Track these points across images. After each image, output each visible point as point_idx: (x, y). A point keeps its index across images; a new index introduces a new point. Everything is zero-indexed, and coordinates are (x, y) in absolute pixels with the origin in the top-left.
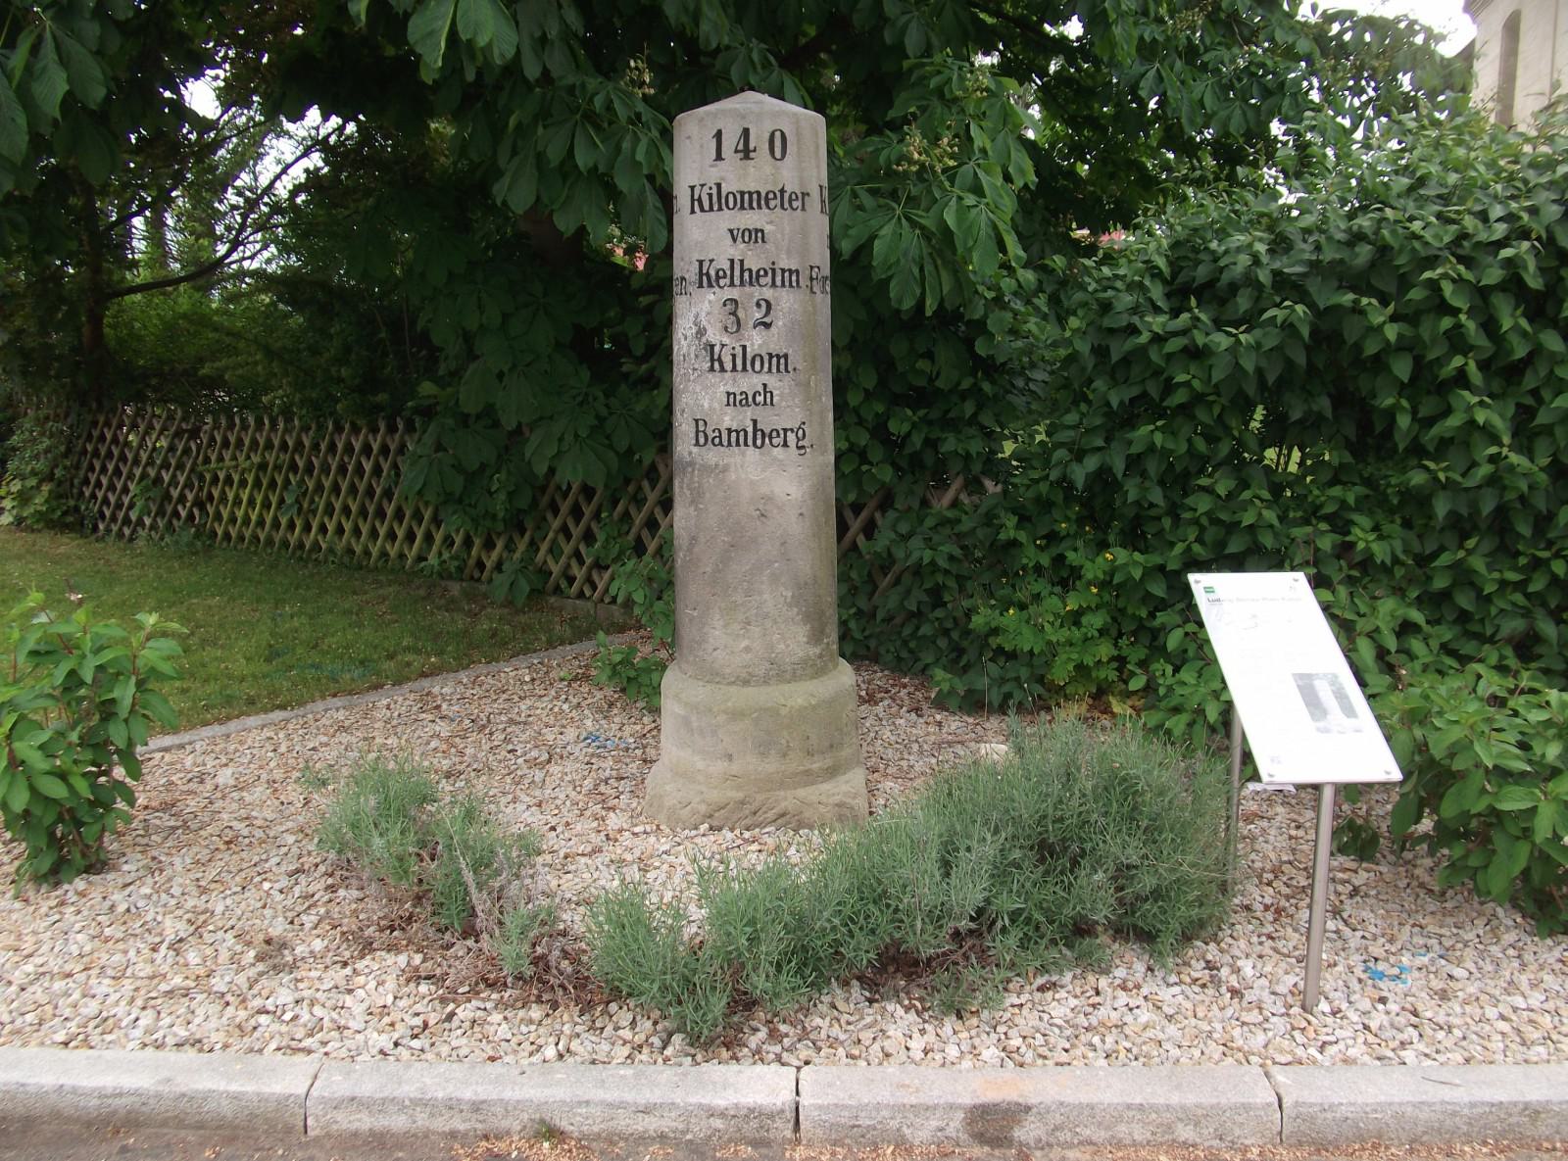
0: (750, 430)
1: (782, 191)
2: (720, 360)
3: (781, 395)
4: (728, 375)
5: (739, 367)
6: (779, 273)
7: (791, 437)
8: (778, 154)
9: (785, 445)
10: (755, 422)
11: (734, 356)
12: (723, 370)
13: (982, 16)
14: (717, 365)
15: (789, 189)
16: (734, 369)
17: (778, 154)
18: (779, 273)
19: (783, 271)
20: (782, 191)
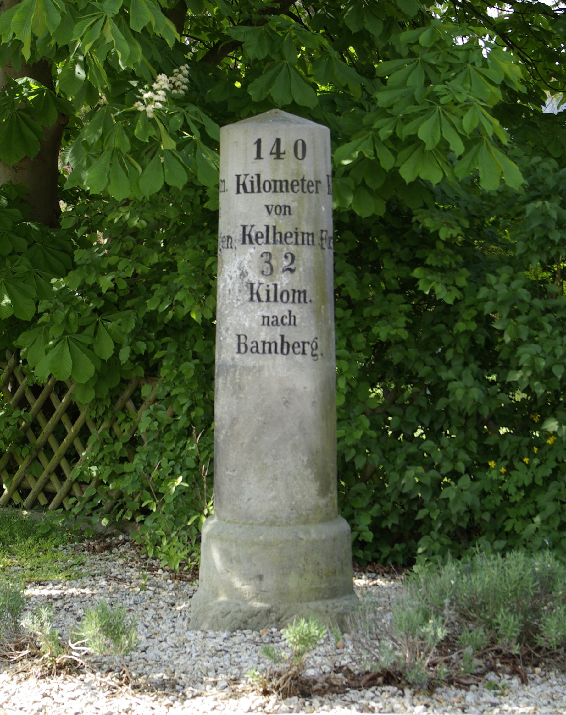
1: (303, 180)
3: (302, 318)
7: (308, 348)
9: (304, 353)
11: (252, 182)
15: (307, 179)
17: (300, 156)
20: (303, 180)
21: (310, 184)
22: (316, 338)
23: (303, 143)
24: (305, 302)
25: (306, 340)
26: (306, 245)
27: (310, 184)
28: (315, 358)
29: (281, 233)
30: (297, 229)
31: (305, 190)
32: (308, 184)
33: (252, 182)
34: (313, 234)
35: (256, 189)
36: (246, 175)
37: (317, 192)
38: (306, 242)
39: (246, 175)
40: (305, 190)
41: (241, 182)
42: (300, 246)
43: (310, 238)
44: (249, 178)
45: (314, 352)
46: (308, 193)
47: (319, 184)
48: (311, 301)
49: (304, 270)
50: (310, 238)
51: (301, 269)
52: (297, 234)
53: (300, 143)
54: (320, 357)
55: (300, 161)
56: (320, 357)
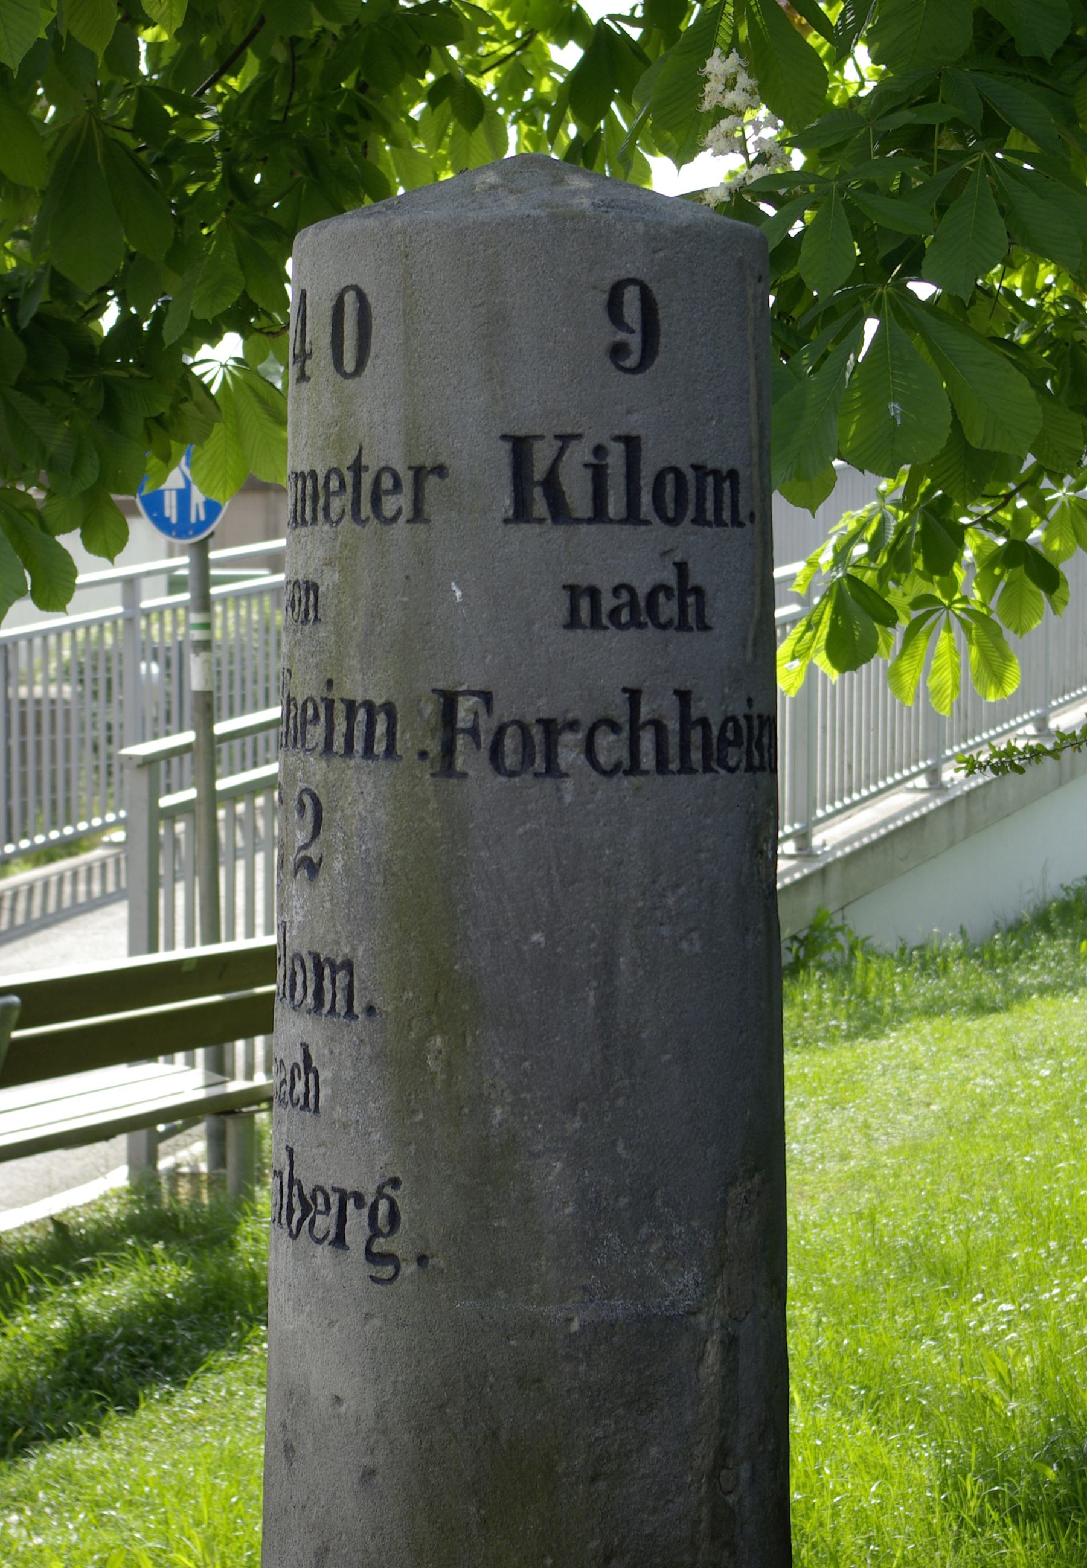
0: (673, 725)
1: (357, 468)
2: (551, 484)
3: (335, 1081)
4: (356, 761)
5: (615, 506)
6: (340, 708)
7: (357, 1221)
8: (349, 365)
9: (339, 1241)
10: (684, 696)
11: (599, 474)
12: (559, 511)
13: (851, 433)
14: (540, 506)
15: (372, 461)
16: (599, 514)
17: (349, 365)
18: (340, 708)
19: (351, 707)
20: (357, 468)
21: (387, 482)
22: (395, 1183)
23: (361, 297)
24: (350, 1012)
25: (349, 1186)
26: (356, 761)
27: (387, 482)
28: (388, 1271)
29: (704, 722)
30: (330, 683)
31: (366, 509)
32: (377, 481)
33: (599, 474)
34: (389, 709)
35: (615, 506)
36: (565, 439)
37: (418, 515)
38: (359, 746)
39: (565, 439)
40: (366, 509)
41: (539, 471)
42: (337, 761)
43: (381, 728)
44: (579, 455)
45: (380, 1245)
46: (374, 522)
47: (432, 481)
48: (370, 1010)
49: (348, 870)
50: (381, 728)
51: (338, 866)
52: (330, 704)
53: (350, 298)
54: (409, 1269)
55: (350, 383)
56: (409, 1269)
